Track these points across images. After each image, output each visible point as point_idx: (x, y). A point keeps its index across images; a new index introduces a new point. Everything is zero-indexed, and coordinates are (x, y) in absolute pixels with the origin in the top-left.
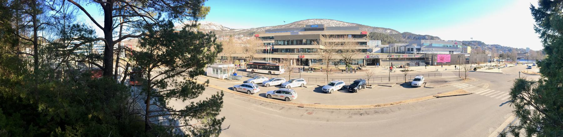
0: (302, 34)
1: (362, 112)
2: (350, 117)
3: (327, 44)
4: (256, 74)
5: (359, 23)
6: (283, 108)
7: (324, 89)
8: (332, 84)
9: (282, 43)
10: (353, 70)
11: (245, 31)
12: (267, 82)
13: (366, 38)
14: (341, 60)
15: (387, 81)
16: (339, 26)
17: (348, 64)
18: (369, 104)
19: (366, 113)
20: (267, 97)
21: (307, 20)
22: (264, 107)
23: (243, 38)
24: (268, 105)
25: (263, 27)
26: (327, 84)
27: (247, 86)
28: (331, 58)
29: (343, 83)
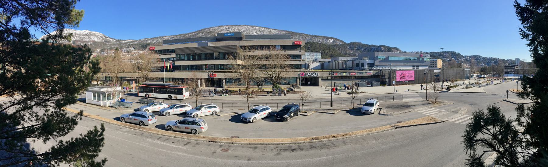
1: (294, 147)
2: (278, 154)
3: (246, 57)
4: (151, 100)
6: (189, 143)
7: (243, 118)
8: (255, 111)
9: (186, 58)
10: (282, 91)
11: (136, 43)
12: (166, 109)
13: (301, 49)
14: (266, 79)
15: (328, 107)
16: (262, 33)
18: (304, 136)
19: (300, 149)
20: (167, 130)
22: (162, 143)
23: (134, 51)
24: (168, 139)
25: (160, 37)
27: (139, 115)
28: (252, 76)
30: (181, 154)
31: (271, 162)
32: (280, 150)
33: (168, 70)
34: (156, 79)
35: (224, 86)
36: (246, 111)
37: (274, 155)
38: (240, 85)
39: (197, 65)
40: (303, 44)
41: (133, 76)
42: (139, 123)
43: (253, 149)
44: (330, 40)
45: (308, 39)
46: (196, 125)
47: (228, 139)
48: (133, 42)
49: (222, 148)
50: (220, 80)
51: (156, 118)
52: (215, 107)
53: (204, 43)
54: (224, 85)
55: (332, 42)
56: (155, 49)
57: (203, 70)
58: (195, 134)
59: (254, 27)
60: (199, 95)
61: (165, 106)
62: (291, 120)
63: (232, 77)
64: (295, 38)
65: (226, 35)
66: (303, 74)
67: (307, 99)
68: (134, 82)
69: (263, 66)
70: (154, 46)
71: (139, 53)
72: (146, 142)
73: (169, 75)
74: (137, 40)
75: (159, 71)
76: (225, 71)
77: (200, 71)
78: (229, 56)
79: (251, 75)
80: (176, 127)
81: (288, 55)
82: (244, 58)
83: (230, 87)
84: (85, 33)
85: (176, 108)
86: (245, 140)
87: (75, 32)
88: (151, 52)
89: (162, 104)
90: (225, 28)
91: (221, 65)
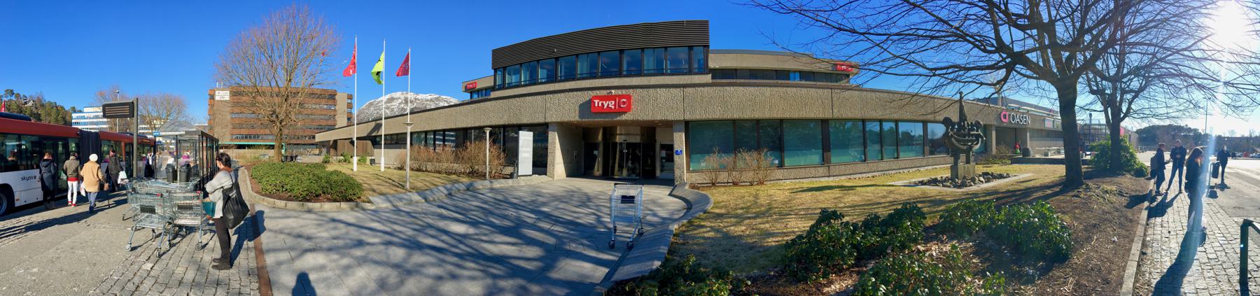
54: (681, 168)
84: (429, 98)
87: (415, 96)
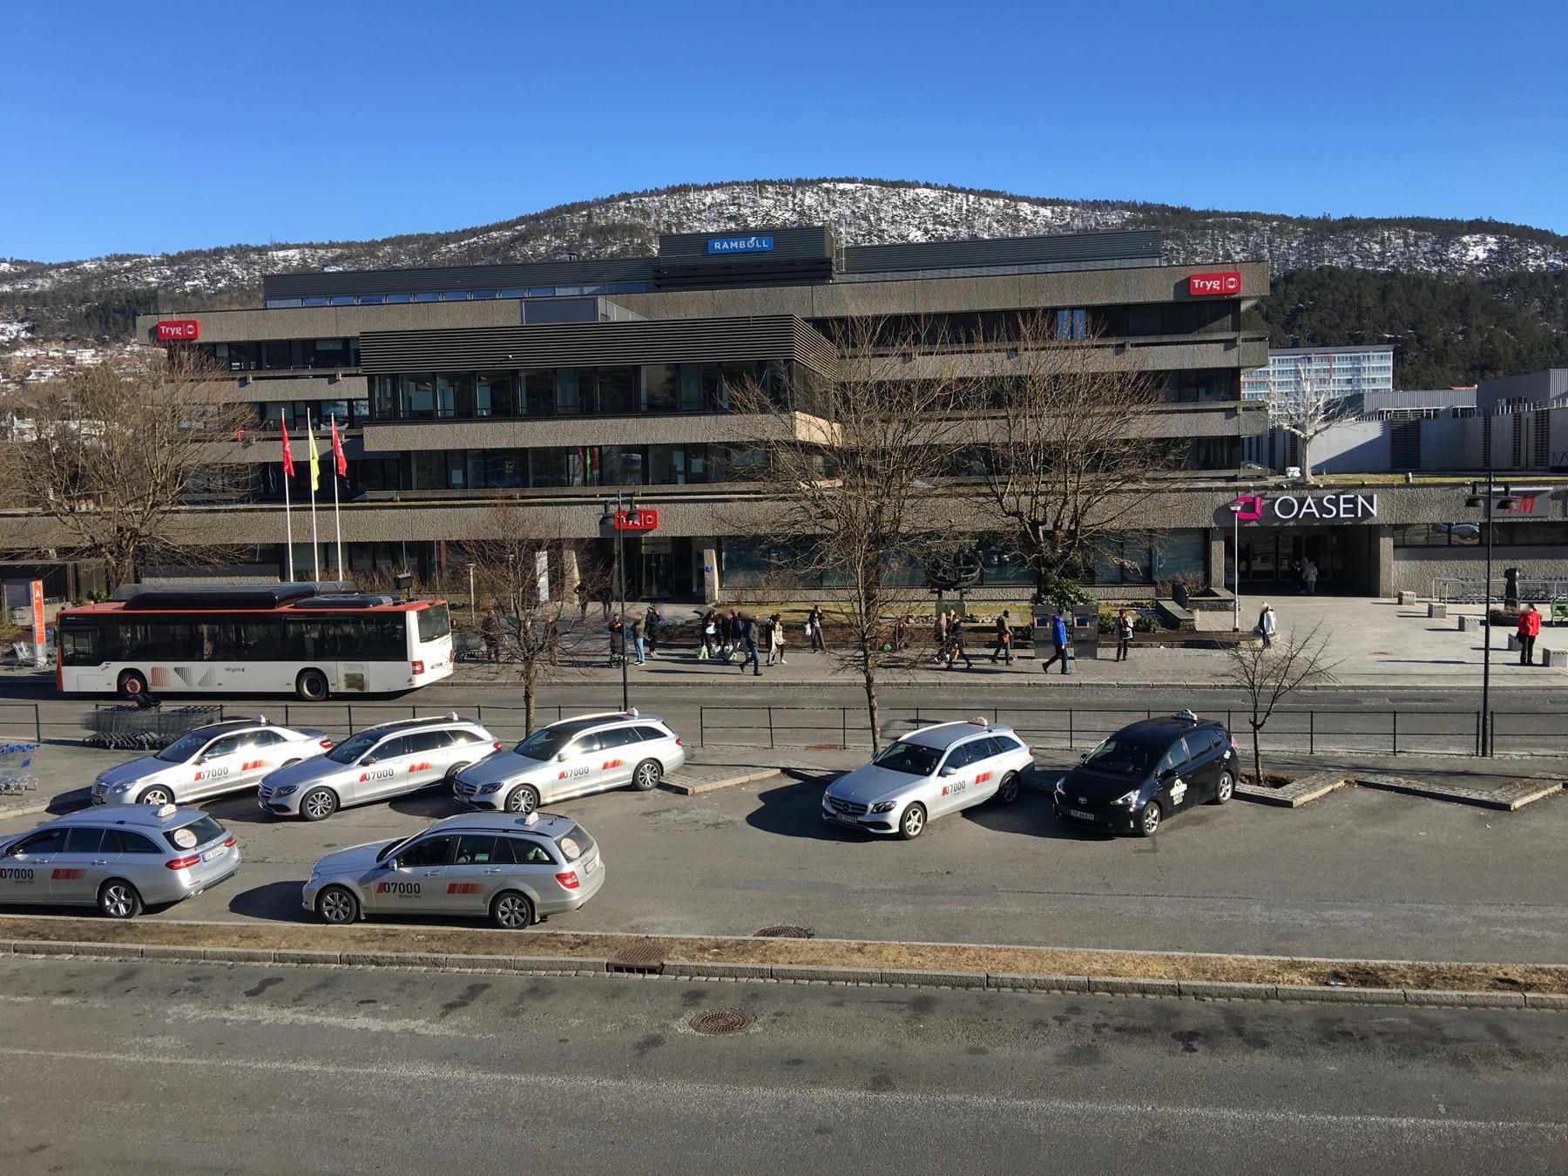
0: (631, 316)
1: (1194, 1014)
2: (1085, 1055)
3: (858, 398)
4: (186, 713)
5: (1155, 199)
6: (475, 990)
7: (842, 804)
8: (918, 761)
9: (445, 399)
10: (1104, 630)
11: (42, 284)
12: (313, 767)
13: (1236, 327)
14: (987, 541)
15: (1456, 752)
16: (964, 232)
17: (1053, 575)
18: (1267, 951)
19: (1239, 1032)
20: (317, 917)
21: (672, 191)
22: (288, 1015)
23: (30, 352)
24: (328, 983)
25: (241, 252)
26: (868, 759)
27: (88, 839)
28: (897, 521)
29: (1018, 746)
30: (423, 1071)
31: (1034, 1104)
32: (1098, 1032)
33: (315, 486)
34: (223, 557)
35: (708, 590)
36: (857, 755)
37: (1058, 1064)
38: (818, 581)
39: (524, 451)
40: (1252, 288)
41: (24, 544)
42: (92, 900)
43: (908, 1013)
44: (1465, 246)
45: (1290, 252)
46: (526, 861)
47: (741, 948)
48: (19, 276)
49: (706, 1008)
50: (685, 552)
51: (229, 842)
52: (655, 734)
53: (567, 300)
55: (1483, 256)
56: (203, 338)
57: (569, 484)
58: (522, 926)
59: (911, 194)
60: (543, 655)
61: (300, 746)
62: (1172, 828)
63: (764, 530)
64: (1195, 253)
65: (717, 245)
66: (1250, 506)
67: (1286, 684)
68: (37, 589)
69: (970, 452)
70: (193, 317)
71: (71, 360)
72: (163, 1033)
73: (326, 526)
74: (51, 267)
75: (241, 501)
76: (715, 487)
77: (547, 491)
78: (744, 386)
79: (887, 515)
80: (382, 888)
81: (1141, 374)
82: (846, 401)
83: (750, 597)
85: (384, 753)
86: (851, 950)
88: (170, 356)
89: (277, 738)
90: (708, 200)
91: (689, 450)
